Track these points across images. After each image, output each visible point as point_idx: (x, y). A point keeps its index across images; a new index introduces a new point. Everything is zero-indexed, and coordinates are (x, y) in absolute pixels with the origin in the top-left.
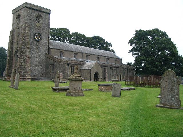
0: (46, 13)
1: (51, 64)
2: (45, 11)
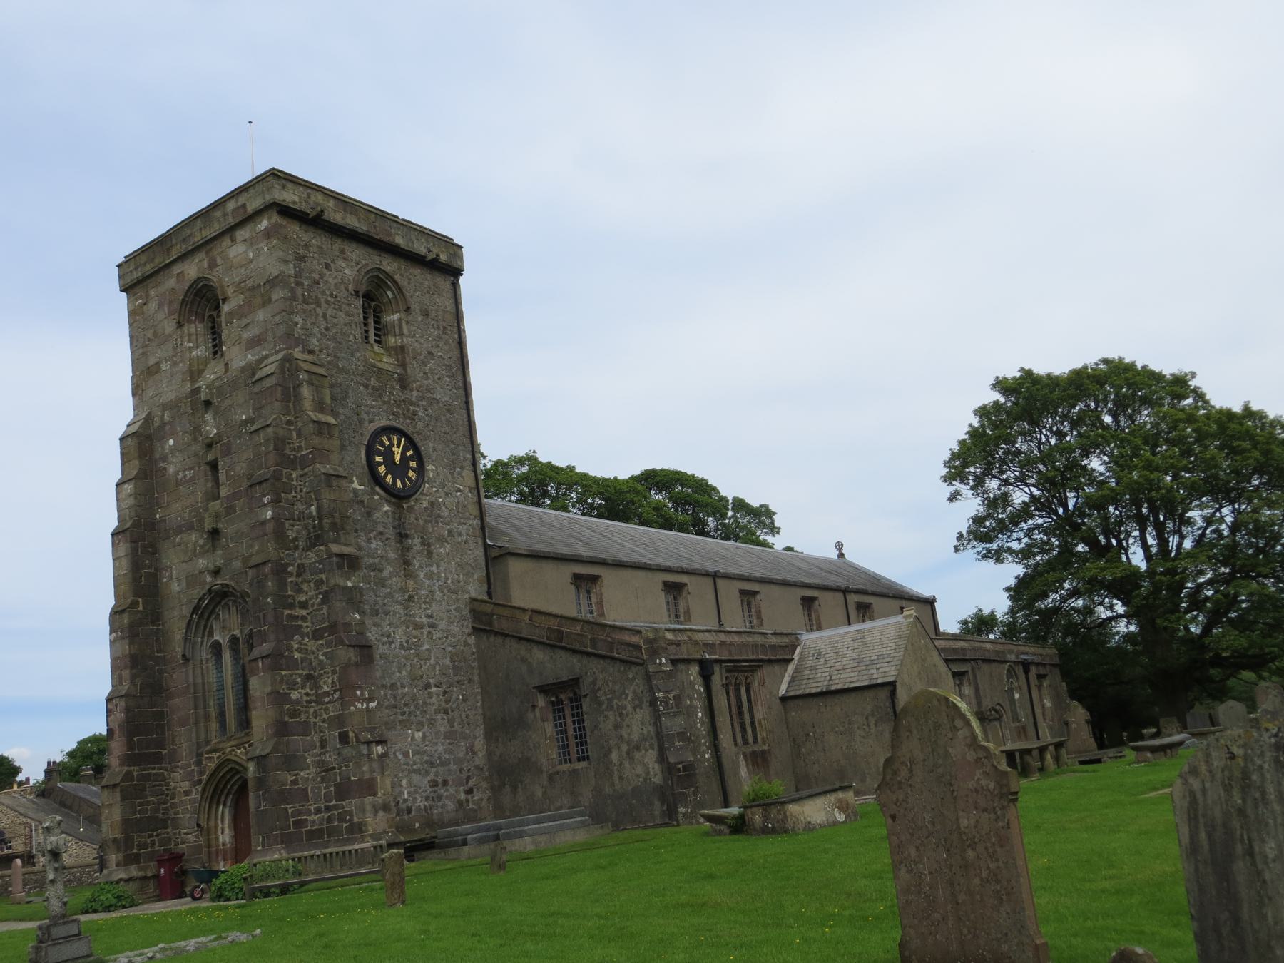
0: (434, 266)
1: (543, 689)
2: (420, 247)
